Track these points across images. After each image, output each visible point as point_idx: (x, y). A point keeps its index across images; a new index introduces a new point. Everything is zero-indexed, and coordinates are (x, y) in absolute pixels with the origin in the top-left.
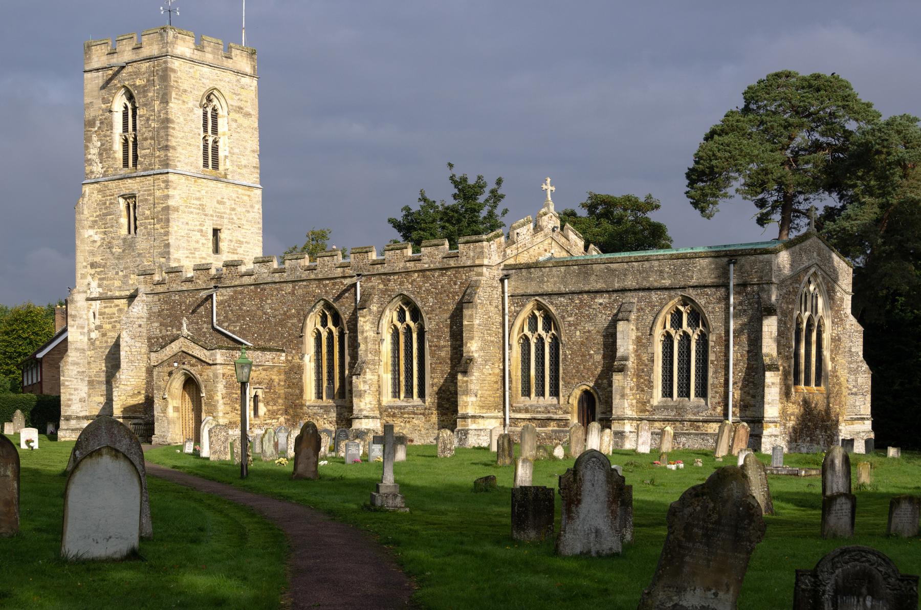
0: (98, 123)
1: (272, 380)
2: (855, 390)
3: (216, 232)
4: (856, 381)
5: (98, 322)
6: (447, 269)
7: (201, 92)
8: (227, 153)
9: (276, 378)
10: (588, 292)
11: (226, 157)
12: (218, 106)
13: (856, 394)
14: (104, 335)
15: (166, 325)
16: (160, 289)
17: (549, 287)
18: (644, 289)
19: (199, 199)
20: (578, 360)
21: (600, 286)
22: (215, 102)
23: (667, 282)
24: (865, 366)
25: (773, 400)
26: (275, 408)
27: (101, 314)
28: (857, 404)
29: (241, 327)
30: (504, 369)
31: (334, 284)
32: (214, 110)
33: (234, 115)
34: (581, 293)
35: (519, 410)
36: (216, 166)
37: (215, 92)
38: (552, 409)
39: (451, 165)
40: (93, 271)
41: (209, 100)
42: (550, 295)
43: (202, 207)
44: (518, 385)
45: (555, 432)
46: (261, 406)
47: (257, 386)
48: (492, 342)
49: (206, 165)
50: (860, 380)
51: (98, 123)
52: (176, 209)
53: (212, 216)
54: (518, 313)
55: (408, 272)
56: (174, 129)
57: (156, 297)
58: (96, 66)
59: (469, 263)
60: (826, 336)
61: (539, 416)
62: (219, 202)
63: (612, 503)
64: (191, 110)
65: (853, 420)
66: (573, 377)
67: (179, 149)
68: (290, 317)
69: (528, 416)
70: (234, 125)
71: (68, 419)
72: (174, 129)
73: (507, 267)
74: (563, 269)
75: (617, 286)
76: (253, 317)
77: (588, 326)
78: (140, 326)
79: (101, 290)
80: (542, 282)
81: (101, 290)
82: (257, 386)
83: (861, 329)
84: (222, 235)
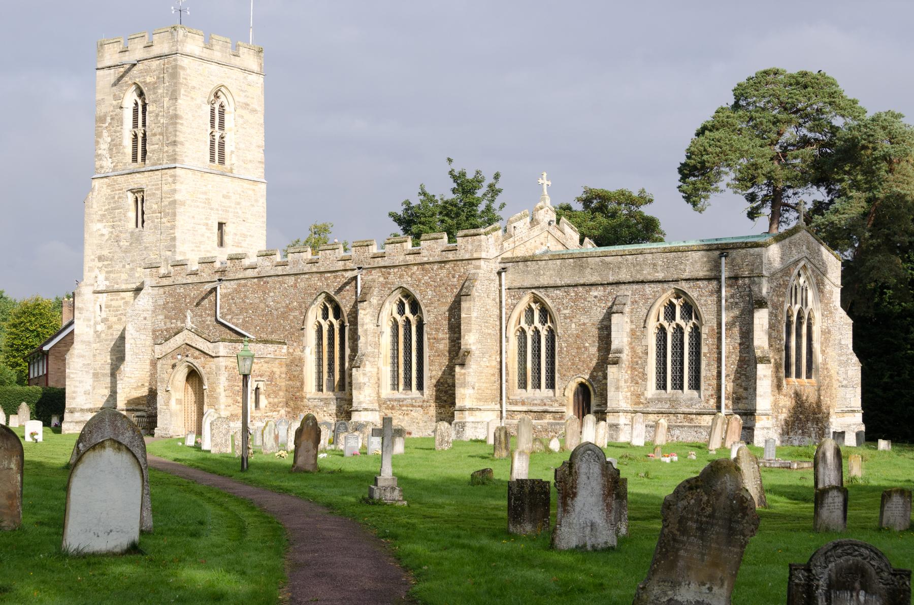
0: (108, 119)
2: (845, 383)
3: (221, 225)
4: (847, 374)
5: (104, 315)
7: (210, 89)
8: (233, 149)
9: (277, 371)
11: (232, 152)
12: (225, 103)
13: (846, 386)
14: (110, 327)
17: (544, 281)
18: (638, 282)
19: (205, 193)
20: (574, 352)
21: (594, 279)
22: (222, 99)
23: (660, 276)
24: (855, 359)
25: (765, 393)
26: (276, 400)
28: (848, 396)
32: (222, 106)
35: (515, 403)
36: (222, 161)
37: (223, 89)
38: (548, 402)
41: (216, 96)
43: (208, 201)
45: (551, 424)
46: (262, 398)
47: (259, 378)
48: (489, 334)
49: (212, 160)
50: (850, 373)
51: (108, 119)
53: (217, 210)
56: (182, 124)
62: (224, 197)
63: (607, 496)
64: (199, 107)
66: (569, 369)
68: (291, 310)
69: (525, 408)
70: (240, 121)
72: (182, 124)
73: (505, 261)
77: (584, 319)
78: (145, 319)
79: (107, 283)
80: (538, 275)
81: (107, 283)
82: (259, 378)
83: (850, 321)
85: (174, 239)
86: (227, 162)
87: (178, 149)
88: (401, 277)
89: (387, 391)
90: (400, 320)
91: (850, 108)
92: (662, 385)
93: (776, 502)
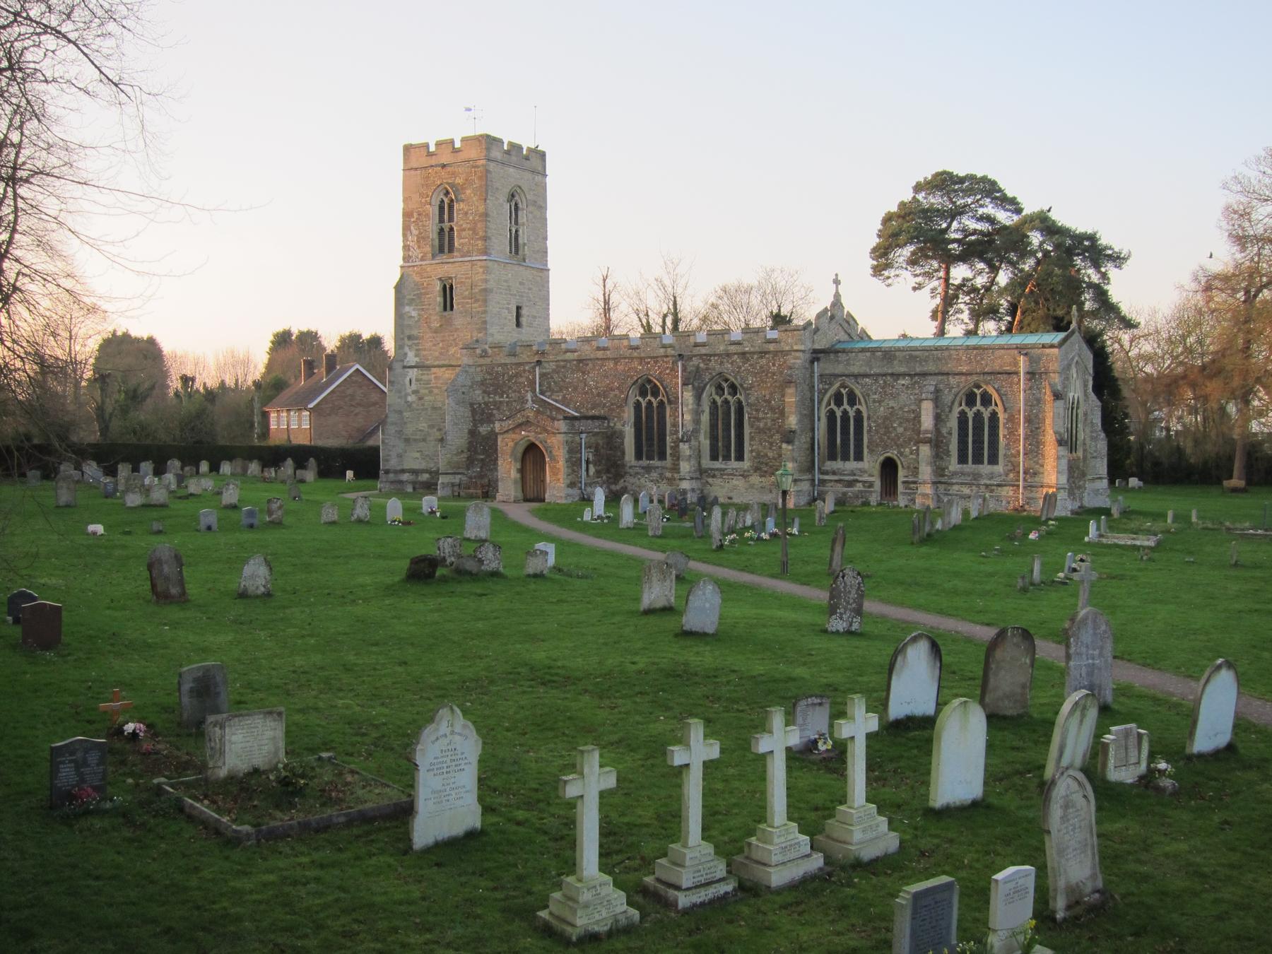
0: (415, 215)
1: (597, 444)
3: (518, 308)
5: (414, 387)
6: (766, 353)
7: (507, 191)
9: (600, 442)
10: (892, 375)
14: (420, 399)
15: (489, 394)
16: (482, 361)
17: (855, 369)
18: (943, 374)
20: (882, 431)
21: (902, 370)
22: (517, 198)
23: (964, 369)
24: (1103, 435)
27: (417, 380)
29: (564, 396)
30: (813, 439)
31: (656, 362)
32: (516, 204)
33: (531, 208)
34: (885, 375)
35: (826, 473)
38: (858, 472)
39: (837, 282)
40: (410, 343)
41: (513, 196)
42: (856, 376)
44: (824, 450)
45: (861, 492)
46: (591, 466)
51: (415, 215)
52: (491, 291)
54: (826, 391)
55: (728, 355)
57: (479, 369)
58: (415, 166)
59: (787, 348)
60: (1081, 412)
61: (846, 478)
62: (521, 283)
63: (489, 486)
64: (501, 205)
65: (1093, 479)
66: (877, 445)
67: (494, 239)
68: (612, 389)
69: (836, 478)
71: (387, 472)
73: (815, 351)
74: (868, 354)
75: (918, 370)
76: (575, 389)
77: (892, 403)
79: (417, 359)
80: (848, 364)
81: (417, 359)
83: (1099, 404)
84: (524, 312)
85: (485, 322)
86: (520, 252)
87: (713, 300)
88: (722, 363)
89: (706, 462)
90: (719, 400)
91: (1011, 204)
92: (962, 459)
93: (554, 473)
